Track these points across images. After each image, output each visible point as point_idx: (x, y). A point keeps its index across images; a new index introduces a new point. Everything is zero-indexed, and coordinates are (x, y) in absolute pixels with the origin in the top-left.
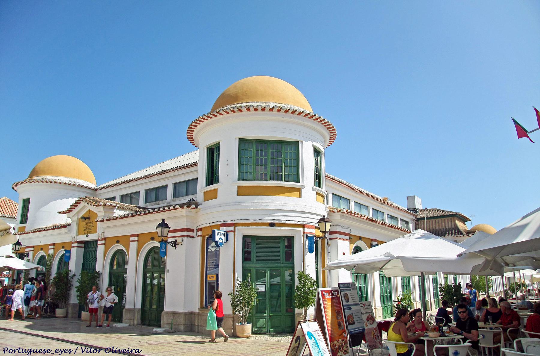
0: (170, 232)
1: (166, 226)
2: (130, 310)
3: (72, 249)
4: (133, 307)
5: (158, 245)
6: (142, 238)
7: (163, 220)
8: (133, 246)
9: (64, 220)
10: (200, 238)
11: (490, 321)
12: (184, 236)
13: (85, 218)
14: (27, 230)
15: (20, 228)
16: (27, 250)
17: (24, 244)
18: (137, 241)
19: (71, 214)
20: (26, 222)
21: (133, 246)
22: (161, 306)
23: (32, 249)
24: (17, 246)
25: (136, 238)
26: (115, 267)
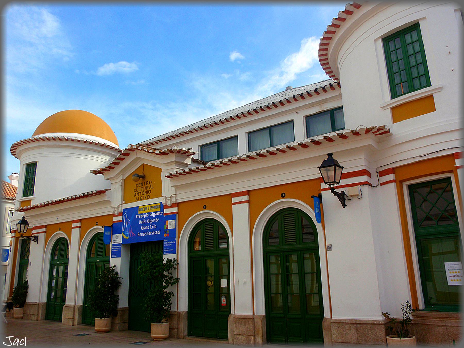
0: (344, 176)
1: (336, 164)
2: (69, 307)
3: (323, 193)
4: (250, 314)
5: (102, 230)
6: (84, 223)
7: (24, 217)
8: (75, 233)
9: (99, 183)
10: (393, 185)
11: (411, 318)
12: (362, 184)
13: (139, 177)
14: (33, 203)
15: (22, 203)
16: (34, 231)
17: (33, 223)
18: (80, 227)
19: (112, 173)
20: (32, 194)
21: (75, 233)
22: (64, 300)
23: (44, 230)
24: (23, 227)
25: (78, 224)
26: (198, 247)
